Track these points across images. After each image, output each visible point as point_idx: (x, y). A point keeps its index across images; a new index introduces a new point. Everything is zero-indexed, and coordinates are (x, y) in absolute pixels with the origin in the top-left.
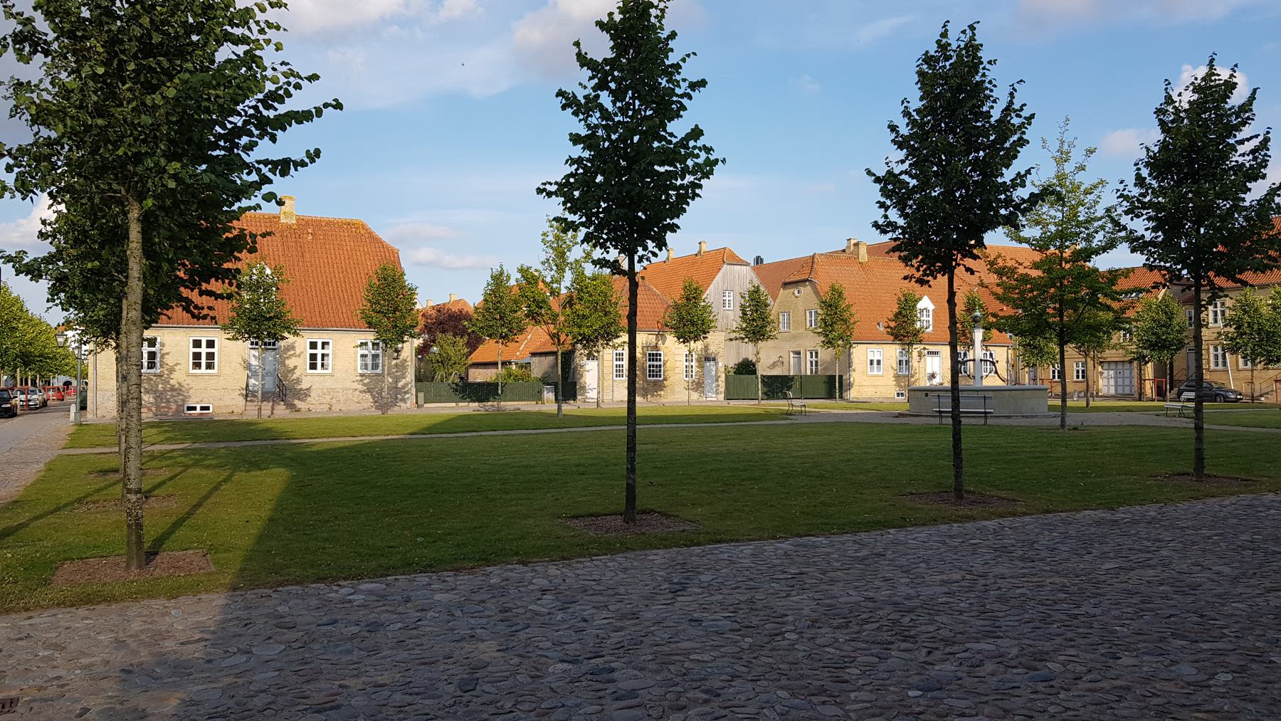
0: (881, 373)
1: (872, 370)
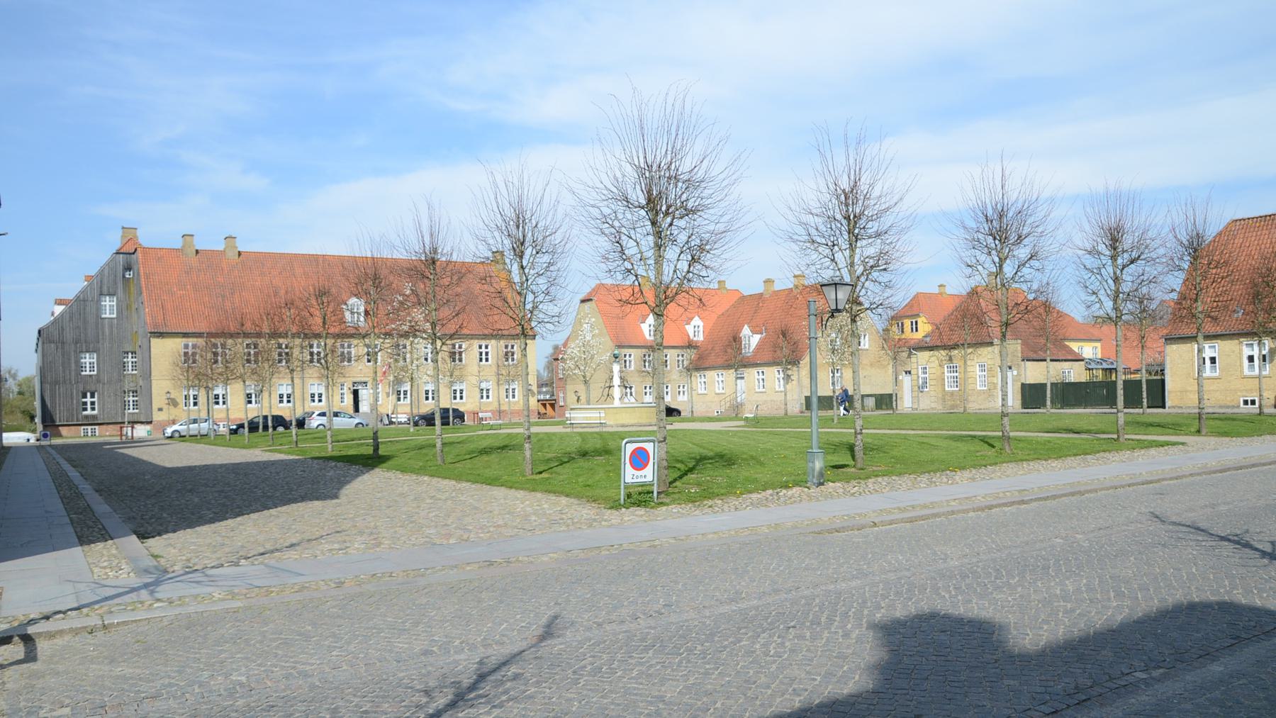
0: (1217, 374)
1: (1252, 367)
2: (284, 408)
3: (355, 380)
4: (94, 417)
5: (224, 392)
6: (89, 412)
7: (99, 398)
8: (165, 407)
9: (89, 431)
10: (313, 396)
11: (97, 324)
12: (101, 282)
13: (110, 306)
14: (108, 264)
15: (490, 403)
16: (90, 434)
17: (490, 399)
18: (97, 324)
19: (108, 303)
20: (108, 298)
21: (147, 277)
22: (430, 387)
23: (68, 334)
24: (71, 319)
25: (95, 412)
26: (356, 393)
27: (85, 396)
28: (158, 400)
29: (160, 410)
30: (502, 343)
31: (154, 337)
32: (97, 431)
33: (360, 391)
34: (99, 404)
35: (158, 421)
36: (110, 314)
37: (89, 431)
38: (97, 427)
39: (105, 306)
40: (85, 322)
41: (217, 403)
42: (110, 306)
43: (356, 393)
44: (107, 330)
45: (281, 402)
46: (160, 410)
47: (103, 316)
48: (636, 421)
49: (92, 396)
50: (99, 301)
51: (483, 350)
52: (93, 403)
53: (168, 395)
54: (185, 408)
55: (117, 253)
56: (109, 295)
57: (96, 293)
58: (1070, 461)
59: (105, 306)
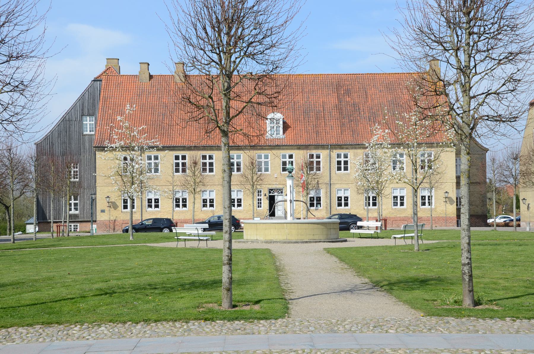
2: (207, 211)
3: (271, 187)
4: (76, 216)
5: (429, 194)
6: (73, 212)
7: (80, 201)
8: (107, 209)
9: (73, 227)
10: (150, 201)
11: (79, 139)
12: (83, 104)
13: (90, 124)
14: (87, 90)
15: (405, 210)
16: (73, 229)
17: (405, 207)
18: (79, 139)
19: (88, 122)
20: (88, 118)
21: (105, 100)
22: (426, 193)
23: (57, 148)
24: (59, 135)
25: (77, 212)
26: (272, 200)
27: (70, 199)
28: (101, 203)
29: (103, 211)
30: (335, 153)
31: (99, 150)
32: (78, 227)
33: (276, 197)
34: (80, 205)
35: (100, 221)
36: (90, 131)
37: (73, 227)
38: (78, 224)
39: (86, 124)
40: (70, 139)
41: (150, 206)
42: (90, 124)
43: (272, 200)
44: (87, 145)
45: (205, 206)
46: (103, 211)
47: (85, 133)
48: (285, 238)
49: (75, 199)
50: (81, 121)
51: (315, 160)
52: (76, 205)
53: (446, 194)
54: (366, 208)
55: (94, 81)
56: (89, 115)
57: (79, 114)
58: (161, 327)
59: (86, 124)
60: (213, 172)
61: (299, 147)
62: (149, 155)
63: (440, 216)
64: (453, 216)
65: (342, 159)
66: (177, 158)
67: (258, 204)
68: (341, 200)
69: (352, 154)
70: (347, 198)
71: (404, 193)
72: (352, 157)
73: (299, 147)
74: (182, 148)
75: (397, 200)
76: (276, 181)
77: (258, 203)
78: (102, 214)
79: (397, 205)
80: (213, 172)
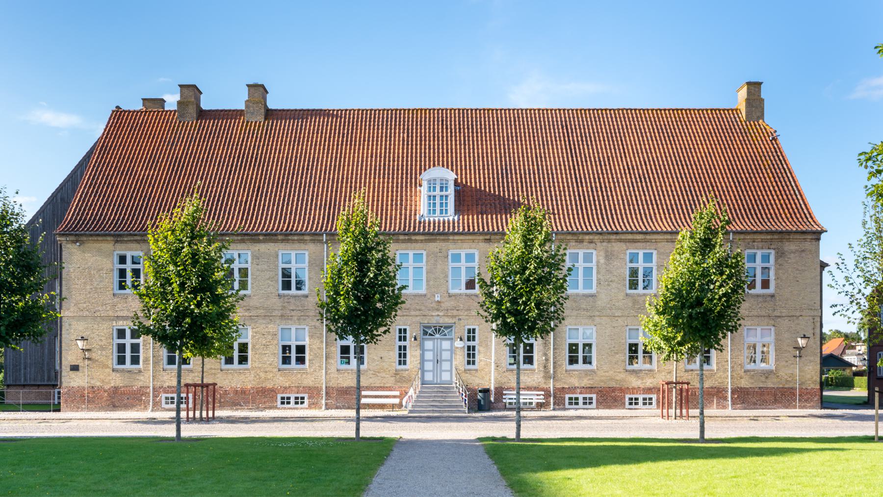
29: (75, 368)
46: (75, 368)
60: (769, 288)
61: (488, 237)
62: (122, 253)
63: (787, 386)
64: (812, 386)
65: (641, 265)
66: (123, 260)
67: (400, 356)
68: (576, 351)
69: (602, 253)
70: (590, 345)
71: (767, 340)
72: (602, 261)
73: (488, 237)
74: (239, 238)
75: (290, 353)
76: (438, 310)
77: (400, 354)
78: (73, 374)
79: (577, 362)
80: (769, 288)
